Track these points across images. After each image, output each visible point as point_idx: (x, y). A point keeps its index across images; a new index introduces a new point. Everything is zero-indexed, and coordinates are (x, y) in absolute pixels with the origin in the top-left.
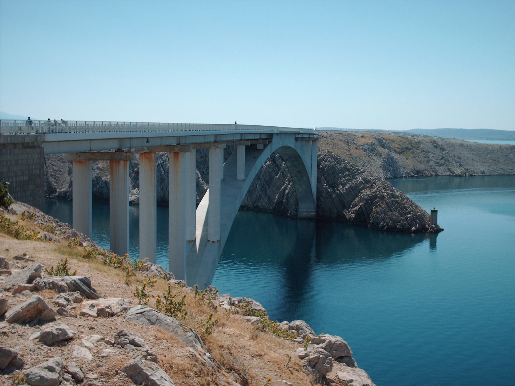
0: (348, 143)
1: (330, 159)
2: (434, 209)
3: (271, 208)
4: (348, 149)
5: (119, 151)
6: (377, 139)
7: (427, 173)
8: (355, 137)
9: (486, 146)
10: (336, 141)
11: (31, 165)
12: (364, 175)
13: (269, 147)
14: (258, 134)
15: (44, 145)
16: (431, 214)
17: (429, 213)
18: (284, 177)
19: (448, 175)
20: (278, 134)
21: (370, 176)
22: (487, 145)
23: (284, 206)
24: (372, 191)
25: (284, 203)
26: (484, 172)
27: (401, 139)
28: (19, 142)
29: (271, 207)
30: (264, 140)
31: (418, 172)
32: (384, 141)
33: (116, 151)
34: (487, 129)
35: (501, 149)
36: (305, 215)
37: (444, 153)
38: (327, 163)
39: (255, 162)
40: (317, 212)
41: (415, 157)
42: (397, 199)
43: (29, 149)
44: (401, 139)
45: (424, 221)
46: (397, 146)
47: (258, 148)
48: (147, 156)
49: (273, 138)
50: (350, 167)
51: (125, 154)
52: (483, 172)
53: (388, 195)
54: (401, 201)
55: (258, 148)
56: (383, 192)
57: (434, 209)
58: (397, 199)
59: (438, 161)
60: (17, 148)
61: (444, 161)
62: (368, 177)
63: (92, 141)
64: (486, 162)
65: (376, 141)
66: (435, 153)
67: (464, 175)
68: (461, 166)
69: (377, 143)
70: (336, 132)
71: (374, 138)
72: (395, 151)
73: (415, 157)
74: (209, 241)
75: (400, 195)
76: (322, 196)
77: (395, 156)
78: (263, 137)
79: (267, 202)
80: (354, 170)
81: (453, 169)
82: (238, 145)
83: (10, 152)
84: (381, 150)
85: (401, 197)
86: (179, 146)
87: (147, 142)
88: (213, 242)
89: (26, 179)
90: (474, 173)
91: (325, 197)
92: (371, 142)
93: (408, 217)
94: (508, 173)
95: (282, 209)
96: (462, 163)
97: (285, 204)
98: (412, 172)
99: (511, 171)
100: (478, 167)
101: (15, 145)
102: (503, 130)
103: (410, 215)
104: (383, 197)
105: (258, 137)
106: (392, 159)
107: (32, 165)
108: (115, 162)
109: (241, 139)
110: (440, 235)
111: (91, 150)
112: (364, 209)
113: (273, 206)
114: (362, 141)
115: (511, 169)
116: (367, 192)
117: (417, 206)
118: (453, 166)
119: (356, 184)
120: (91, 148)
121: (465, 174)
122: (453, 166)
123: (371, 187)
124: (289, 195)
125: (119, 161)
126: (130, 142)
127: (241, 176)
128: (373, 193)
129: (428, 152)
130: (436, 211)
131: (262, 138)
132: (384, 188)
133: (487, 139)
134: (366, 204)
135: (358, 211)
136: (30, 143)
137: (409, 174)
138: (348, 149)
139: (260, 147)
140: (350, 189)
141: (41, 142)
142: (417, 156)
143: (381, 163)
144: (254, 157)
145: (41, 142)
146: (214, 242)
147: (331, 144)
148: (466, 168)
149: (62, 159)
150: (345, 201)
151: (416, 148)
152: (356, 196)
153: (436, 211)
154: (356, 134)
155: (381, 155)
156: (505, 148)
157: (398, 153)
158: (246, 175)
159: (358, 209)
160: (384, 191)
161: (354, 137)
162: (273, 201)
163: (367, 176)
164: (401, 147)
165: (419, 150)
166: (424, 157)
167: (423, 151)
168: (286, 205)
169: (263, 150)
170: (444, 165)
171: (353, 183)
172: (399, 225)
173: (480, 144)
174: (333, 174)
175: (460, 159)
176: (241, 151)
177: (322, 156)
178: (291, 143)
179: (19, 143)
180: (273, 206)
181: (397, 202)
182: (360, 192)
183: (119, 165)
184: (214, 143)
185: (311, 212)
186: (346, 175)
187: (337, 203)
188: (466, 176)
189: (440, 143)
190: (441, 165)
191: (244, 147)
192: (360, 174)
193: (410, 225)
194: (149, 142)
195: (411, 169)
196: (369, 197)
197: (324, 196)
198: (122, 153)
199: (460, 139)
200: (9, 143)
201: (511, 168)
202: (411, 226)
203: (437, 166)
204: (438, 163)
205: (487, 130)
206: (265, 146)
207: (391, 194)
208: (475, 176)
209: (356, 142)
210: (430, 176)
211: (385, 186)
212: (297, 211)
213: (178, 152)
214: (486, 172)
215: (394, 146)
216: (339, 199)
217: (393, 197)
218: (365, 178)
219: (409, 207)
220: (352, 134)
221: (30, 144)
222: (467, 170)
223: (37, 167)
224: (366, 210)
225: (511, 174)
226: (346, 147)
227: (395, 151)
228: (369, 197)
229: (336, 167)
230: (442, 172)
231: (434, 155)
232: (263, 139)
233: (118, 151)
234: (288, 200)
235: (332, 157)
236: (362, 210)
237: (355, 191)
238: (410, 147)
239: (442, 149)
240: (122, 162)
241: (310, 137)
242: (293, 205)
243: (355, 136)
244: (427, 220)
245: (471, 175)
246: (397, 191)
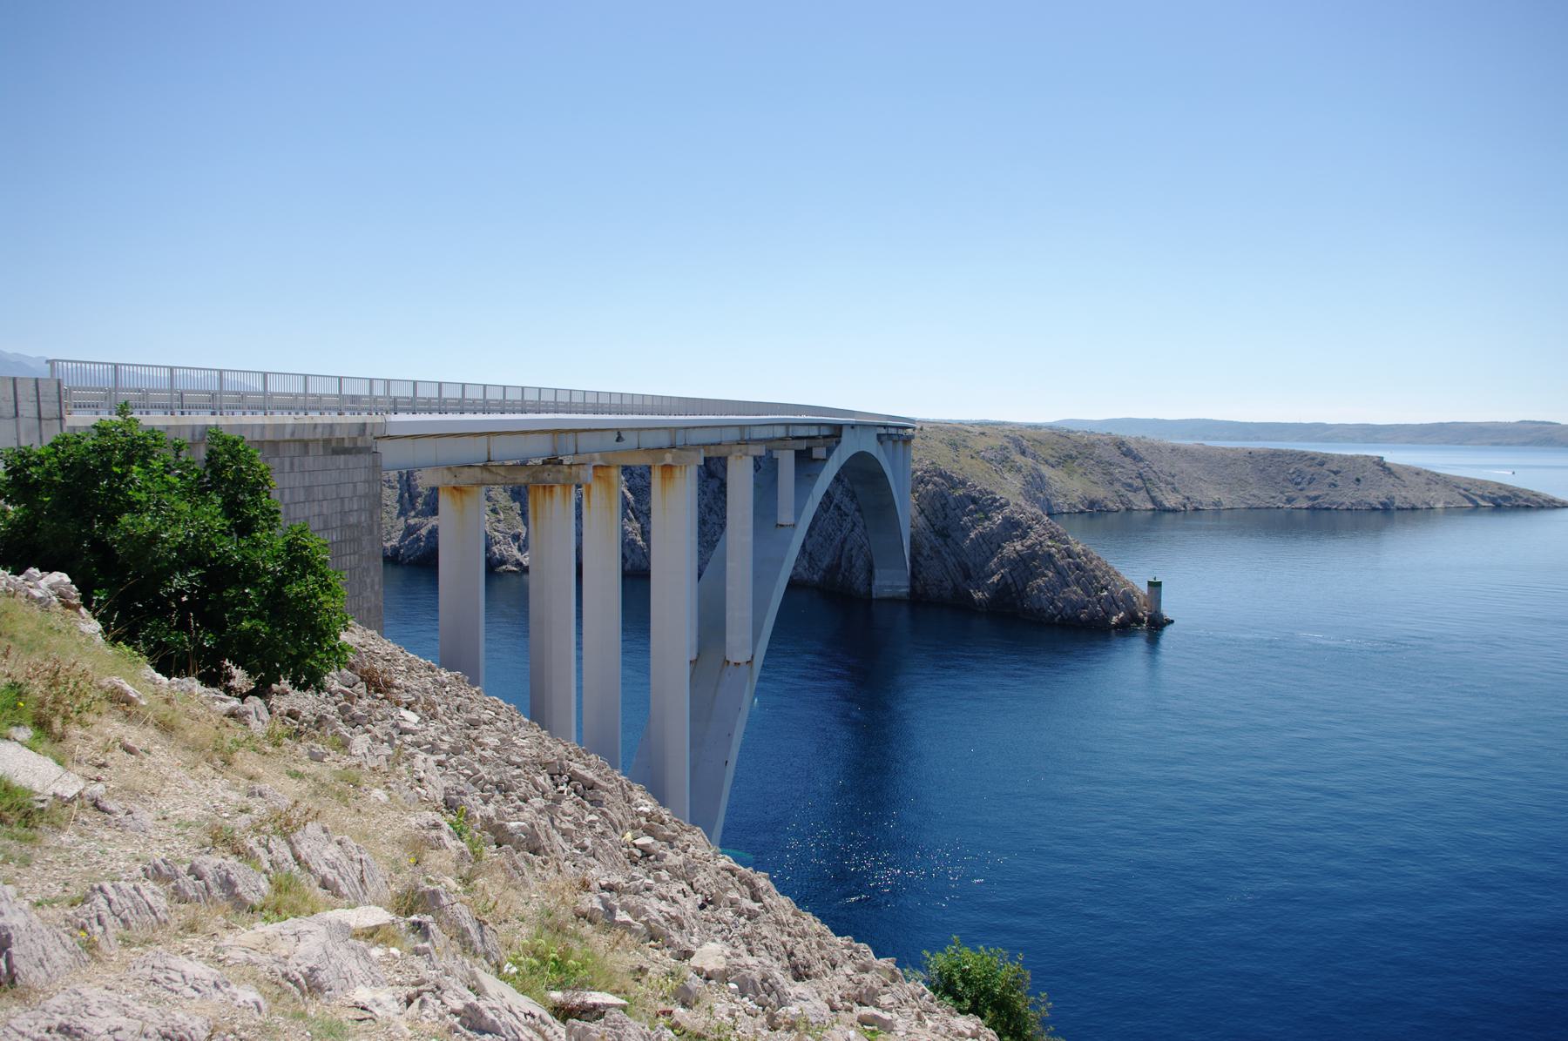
0: (954, 446)
1: (936, 478)
2: (1152, 580)
3: (816, 577)
4: (955, 458)
5: (553, 461)
6: (1011, 438)
7: (1111, 505)
8: (968, 434)
9: (1223, 451)
10: (932, 443)
11: (346, 501)
12: (1007, 511)
13: (836, 453)
14: (814, 427)
15: (382, 446)
16: (1149, 589)
17: (1144, 589)
18: (841, 516)
19: (1151, 510)
20: (853, 426)
21: (1021, 514)
22: (1223, 448)
23: (844, 575)
24: (1026, 544)
25: (843, 569)
26: (1220, 502)
27: (1056, 438)
28: (317, 437)
29: (815, 576)
30: (828, 440)
31: (1092, 504)
32: (1025, 442)
33: (544, 463)
34: (1212, 420)
35: (1253, 457)
36: (887, 593)
37: (1141, 465)
38: (930, 487)
39: (813, 485)
40: (912, 587)
41: (1085, 474)
42: (1078, 560)
43: (342, 456)
44: (1056, 438)
45: (1134, 604)
46: (1051, 452)
47: (815, 456)
48: (602, 475)
49: (843, 435)
50: (977, 495)
51: (566, 470)
52: (1217, 503)
53: (1059, 552)
54: (1085, 563)
55: (815, 456)
56: (1048, 546)
57: (1155, 579)
58: (1078, 560)
59: (1130, 481)
60: (311, 454)
61: (1145, 483)
62: (1015, 515)
63: (492, 438)
64: (1225, 483)
65: (1009, 442)
66: (1124, 465)
67: (1183, 509)
68: (1175, 490)
69: (1011, 446)
70: (932, 425)
71: (1005, 436)
72: (1046, 462)
73: (1085, 474)
74: (728, 662)
75: (1084, 551)
76: (920, 554)
77: (1046, 471)
78: (825, 431)
79: (807, 566)
80: (987, 500)
81: (1160, 497)
82: (778, 449)
83: (292, 464)
84: (1019, 460)
85: (1086, 556)
86: (674, 450)
87: (617, 440)
88: (735, 664)
89: (334, 538)
90: (1201, 503)
91: (928, 556)
92: (1000, 444)
93: (1102, 598)
94: (1268, 505)
95: (839, 581)
96: (1177, 485)
97: (846, 571)
98: (1082, 503)
99: (1272, 500)
100: (1209, 494)
101: (305, 444)
102: (1235, 420)
103: (1106, 593)
104: (1050, 555)
105: (814, 432)
106: (1041, 477)
107: (351, 499)
108: (541, 490)
109: (742, 439)
110: (1168, 631)
111: (489, 461)
112: (1010, 581)
113: (819, 574)
114: (980, 444)
115: (1273, 497)
116: (1013, 548)
117: (1117, 574)
118: (1161, 490)
119: (991, 529)
120: (489, 453)
121: (1184, 507)
122: (1161, 490)
123: (1023, 537)
124: (854, 553)
125: (552, 487)
126: (638, 436)
127: (785, 517)
128: (1029, 547)
129: (1110, 464)
130: (1159, 584)
131: (822, 434)
132: (1050, 538)
133: (1229, 439)
134: (1014, 570)
135: (998, 584)
136: (346, 441)
137: (1075, 507)
138: (955, 458)
139: (818, 453)
140: (980, 540)
141: (375, 438)
142: (1090, 473)
143: (1020, 486)
144: (809, 476)
145: (375, 438)
146: (739, 664)
147: (923, 449)
148: (1186, 494)
149: (389, 481)
150: (970, 565)
151: (1086, 455)
152: (993, 554)
153: (1159, 584)
154: (970, 429)
155: (1019, 470)
156: (1259, 456)
157: (1053, 467)
158: (798, 513)
159: (998, 581)
160: (1050, 544)
161: (966, 434)
162: (819, 563)
163: (1012, 512)
164: (1057, 455)
165: (1092, 459)
166: (1105, 474)
167: (1101, 462)
168: (847, 574)
169: (825, 460)
170: (1141, 488)
171: (985, 528)
172: (1084, 612)
173: (1211, 448)
174: (944, 510)
175: (1173, 476)
176: (787, 461)
177: (919, 473)
178: (871, 446)
179: (318, 440)
180: (819, 574)
181: (1078, 567)
182: (1000, 546)
183: (551, 497)
184: (738, 444)
185: (898, 587)
186: (970, 510)
187: (953, 567)
188: (1185, 511)
189: (1133, 446)
190: (1136, 490)
191: (792, 453)
192: (998, 508)
193: (1107, 613)
194: (623, 440)
195: (1079, 497)
196: (1019, 555)
197: (925, 554)
198: (560, 467)
199: (1152, 436)
200: (289, 441)
201: (1274, 495)
202: (1108, 614)
203: (1130, 491)
204: (1130, 485)
205: (1232, 422)
206: (830, 451)
207: (1065, 550)
208: (1203, 510)
209: (970, 444)
210: (1117, 511)
211: (1052, 533)
212: (870, 585)
213: (674, 464)
214: (1224, 503)
215: (1044, 452)
216: (957, 559)
217: (1069, 557)
218: (1010, 517)
219: (1104, 576)
220: (961, 430)
221: (347, 444)
222: (1188, 498)
223: (363, 507)
224: (1014, 582)
225: (1273, 506)
226: (953, 454)
227: (1046, 462)
228: (1019, 555)
229: (950, 494)
230: (1139, 504)
231: (1122, 470)
232: (825, 437)
233: (549, 463)
234: (850, 562)
235: (941, 475)
236: (1006, 583)
237: (992, 543)
238: (1074, 453)
239: (1137, 458)
240: (558, 490)
241: (890, 432)
242: (861, 574)
243: (969, 432)
244: (1140, 604)
245: (1197, 509)
246: (1078, 543)
